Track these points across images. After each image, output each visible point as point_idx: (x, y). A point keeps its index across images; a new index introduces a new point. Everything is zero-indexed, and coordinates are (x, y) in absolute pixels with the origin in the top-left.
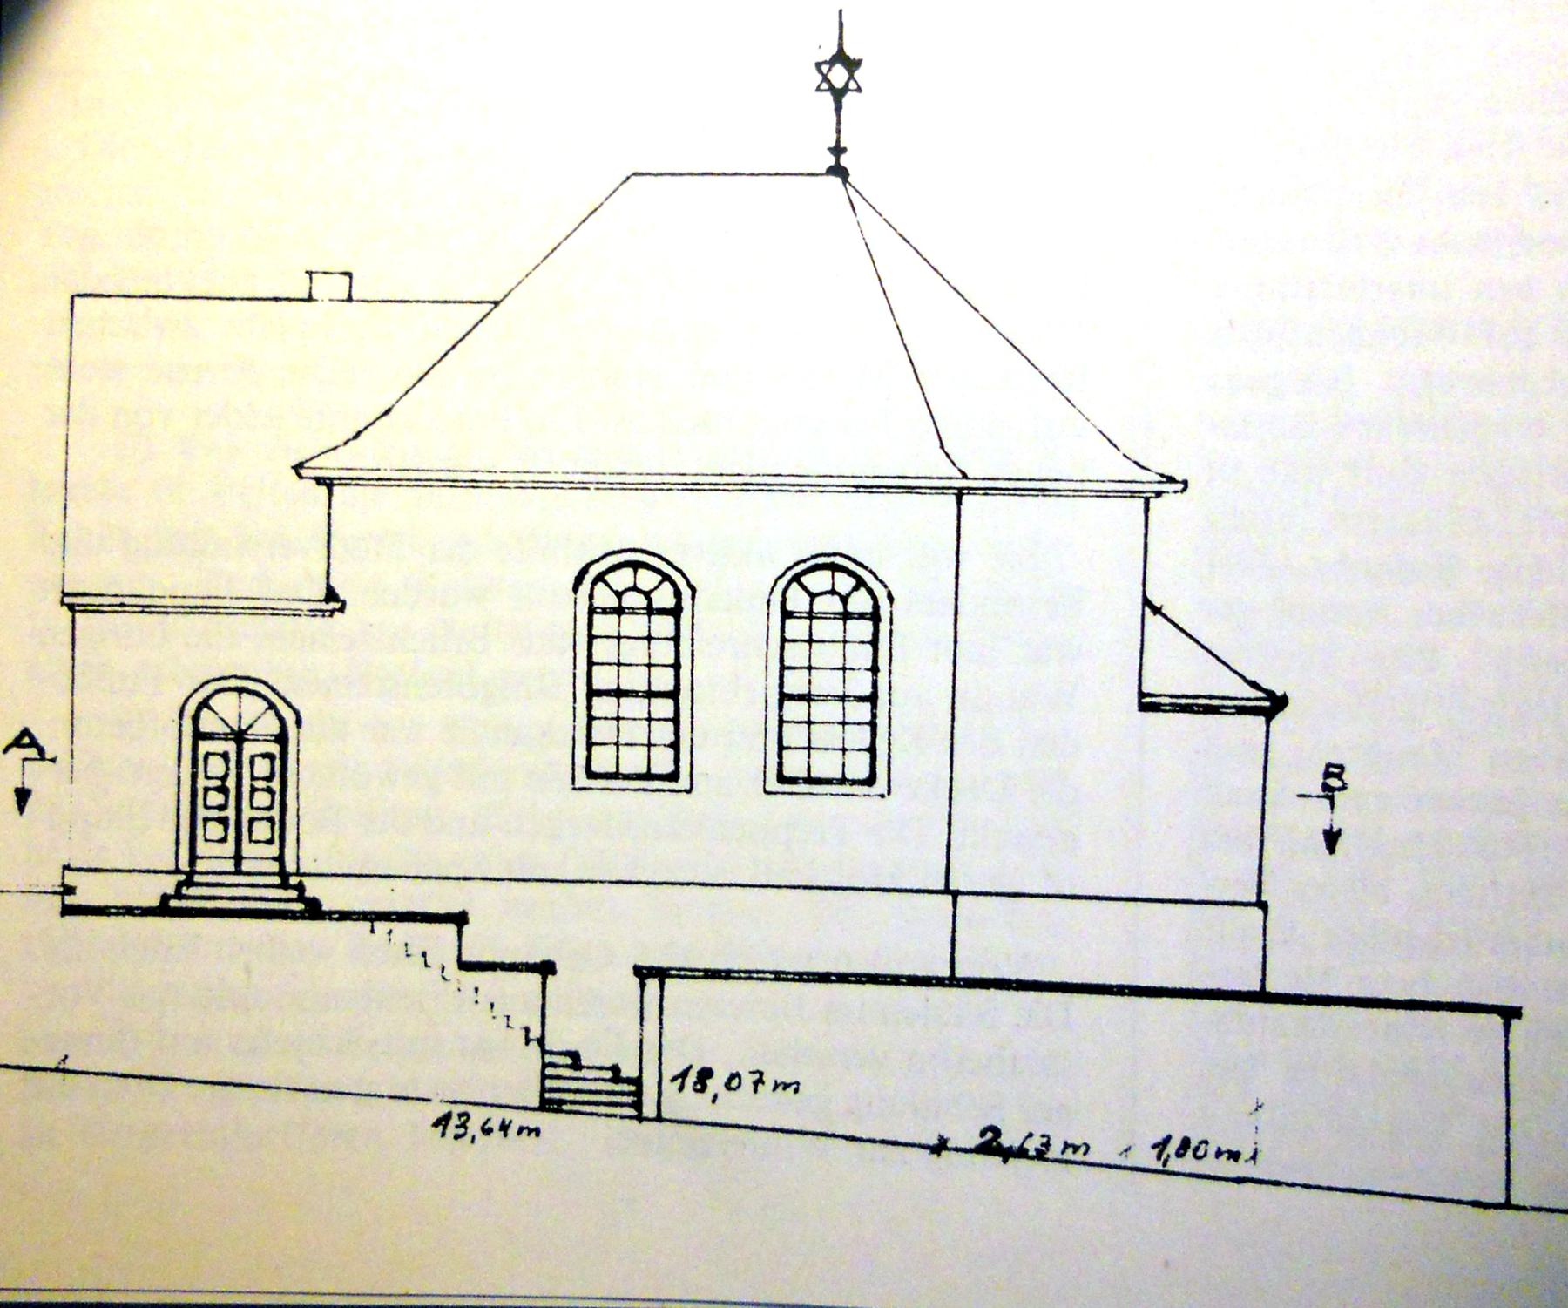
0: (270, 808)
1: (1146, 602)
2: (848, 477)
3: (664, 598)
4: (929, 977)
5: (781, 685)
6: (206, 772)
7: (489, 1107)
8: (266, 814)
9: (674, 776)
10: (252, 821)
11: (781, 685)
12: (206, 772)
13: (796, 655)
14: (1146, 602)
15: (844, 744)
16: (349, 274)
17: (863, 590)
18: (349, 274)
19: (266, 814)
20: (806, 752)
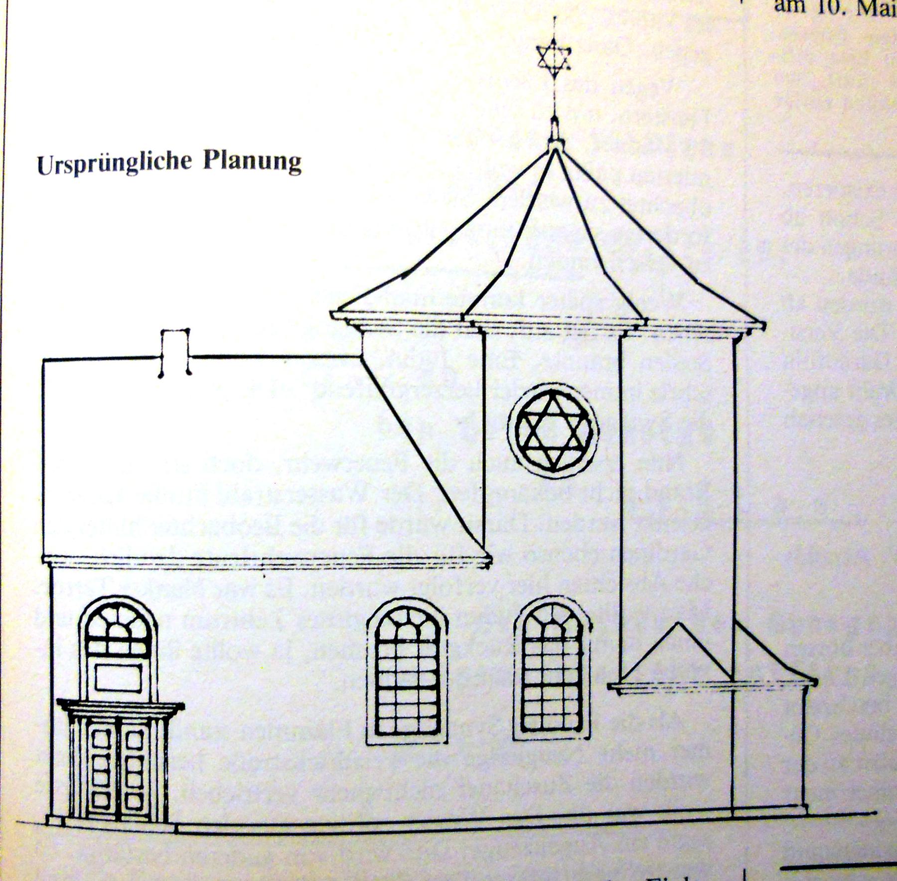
0: (108, 786)
1: (735, 622)
2: (157, 730)
3: (428, 631)
4: (116, 791)
5: (523, 679)
6: (127, 744)
7: (117, 829)
8: (104, 790)
9: (524, 729)
10: (127, 795)
11: (523, 679)
12: (127, 744)
13: (531, 662)
14: (735, 622)
15: (530, 715)
16: (163, 332)
17: (527, 636)
18: (163, 332)
19: (104, 790)
20: (545, 717)
